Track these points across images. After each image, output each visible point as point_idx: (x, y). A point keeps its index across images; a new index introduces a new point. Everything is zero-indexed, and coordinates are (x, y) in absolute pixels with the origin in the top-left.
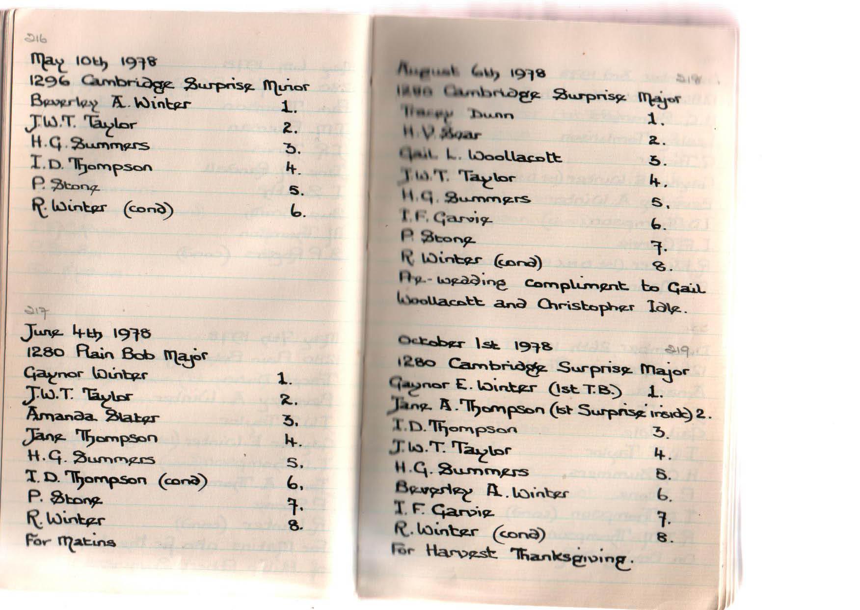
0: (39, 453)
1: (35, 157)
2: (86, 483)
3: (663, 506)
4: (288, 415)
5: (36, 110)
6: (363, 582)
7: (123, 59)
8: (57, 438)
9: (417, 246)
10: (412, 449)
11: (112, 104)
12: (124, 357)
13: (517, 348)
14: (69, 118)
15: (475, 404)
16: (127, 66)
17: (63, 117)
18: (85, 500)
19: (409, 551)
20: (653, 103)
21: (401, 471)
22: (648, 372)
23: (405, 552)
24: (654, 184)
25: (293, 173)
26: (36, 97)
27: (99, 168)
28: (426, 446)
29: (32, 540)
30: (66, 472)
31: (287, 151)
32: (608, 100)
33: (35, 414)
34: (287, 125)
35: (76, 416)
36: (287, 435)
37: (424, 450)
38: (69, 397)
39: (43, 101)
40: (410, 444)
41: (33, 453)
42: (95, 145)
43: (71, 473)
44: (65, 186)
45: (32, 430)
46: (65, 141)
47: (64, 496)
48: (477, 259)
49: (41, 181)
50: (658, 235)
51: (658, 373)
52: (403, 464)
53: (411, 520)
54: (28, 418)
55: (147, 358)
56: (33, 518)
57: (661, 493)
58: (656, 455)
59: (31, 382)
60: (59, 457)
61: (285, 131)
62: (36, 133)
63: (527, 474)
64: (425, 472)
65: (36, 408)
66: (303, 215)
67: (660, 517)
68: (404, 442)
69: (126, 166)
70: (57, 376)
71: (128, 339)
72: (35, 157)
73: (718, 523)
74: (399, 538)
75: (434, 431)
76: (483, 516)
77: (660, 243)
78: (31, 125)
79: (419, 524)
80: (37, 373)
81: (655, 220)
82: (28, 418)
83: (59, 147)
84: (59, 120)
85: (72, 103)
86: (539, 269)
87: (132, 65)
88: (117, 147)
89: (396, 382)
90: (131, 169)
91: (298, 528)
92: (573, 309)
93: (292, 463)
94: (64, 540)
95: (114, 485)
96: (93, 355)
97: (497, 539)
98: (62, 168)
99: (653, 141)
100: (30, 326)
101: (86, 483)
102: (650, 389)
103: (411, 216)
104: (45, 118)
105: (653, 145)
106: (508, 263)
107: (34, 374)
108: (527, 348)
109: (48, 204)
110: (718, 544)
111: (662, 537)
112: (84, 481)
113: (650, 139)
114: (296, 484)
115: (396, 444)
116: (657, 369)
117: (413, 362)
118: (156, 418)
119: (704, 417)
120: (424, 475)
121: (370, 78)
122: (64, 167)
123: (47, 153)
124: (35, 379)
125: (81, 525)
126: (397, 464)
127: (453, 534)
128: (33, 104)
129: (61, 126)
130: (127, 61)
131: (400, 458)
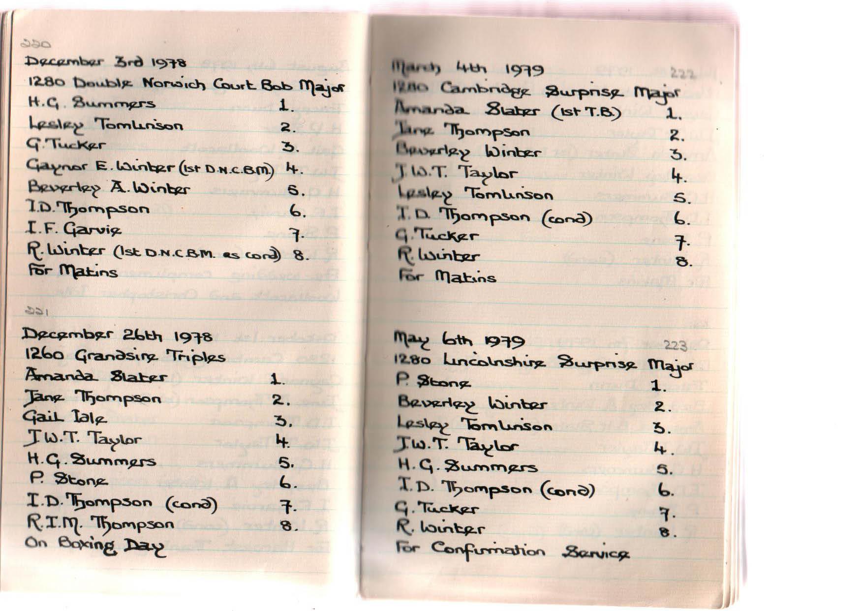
0: (38, 455)
3: (665, 502)
6: (366, 582)
8: (56, 399)
9: (416, 243)
10: (416, 446)
11: (111, 189)
22: (656, 367)
25: (284, 447)
26: (33, 183)
28: (60, 436)
29: (51, 229)
34: (674, 132)
35: (77, 376)
38: (75, 440)
42: (97, 461)
45: (32, 392)
51: (667, 368)
52: (407, 460)
53: (417, 516)
54: (27, 379)
56: (34, 521)
57: (663, 489)
59: (30, 425)
60: (57, 461)
62: (403, 455)
64: (431, 469)
65: (36, 369)
72: (32, 495)
73: (721, 518)
74: (401, 536)
76: (460, 386)
79: (422, 523)
80: (37, 417)
82: (27, 379)
84: (429, 170)
89: (33, 164)
92: (157, 128)
93: (284, 462)
94: (66, 268)
97: (545, 223)
99: (659, 407)
102: (281, 103)
104: (46, 434)
107: (34, 417)
109: (43, 248)
110: (722, 538)
111: (664, 532)
115: (401, 440)
116: (666, 364)
120: (429, 471)
121: (368, 192)
124: (35, 423)
125: (83, 500)
126: (400, 460)
127: (458, 532)
128: (31, 190)
130: (181, 335)
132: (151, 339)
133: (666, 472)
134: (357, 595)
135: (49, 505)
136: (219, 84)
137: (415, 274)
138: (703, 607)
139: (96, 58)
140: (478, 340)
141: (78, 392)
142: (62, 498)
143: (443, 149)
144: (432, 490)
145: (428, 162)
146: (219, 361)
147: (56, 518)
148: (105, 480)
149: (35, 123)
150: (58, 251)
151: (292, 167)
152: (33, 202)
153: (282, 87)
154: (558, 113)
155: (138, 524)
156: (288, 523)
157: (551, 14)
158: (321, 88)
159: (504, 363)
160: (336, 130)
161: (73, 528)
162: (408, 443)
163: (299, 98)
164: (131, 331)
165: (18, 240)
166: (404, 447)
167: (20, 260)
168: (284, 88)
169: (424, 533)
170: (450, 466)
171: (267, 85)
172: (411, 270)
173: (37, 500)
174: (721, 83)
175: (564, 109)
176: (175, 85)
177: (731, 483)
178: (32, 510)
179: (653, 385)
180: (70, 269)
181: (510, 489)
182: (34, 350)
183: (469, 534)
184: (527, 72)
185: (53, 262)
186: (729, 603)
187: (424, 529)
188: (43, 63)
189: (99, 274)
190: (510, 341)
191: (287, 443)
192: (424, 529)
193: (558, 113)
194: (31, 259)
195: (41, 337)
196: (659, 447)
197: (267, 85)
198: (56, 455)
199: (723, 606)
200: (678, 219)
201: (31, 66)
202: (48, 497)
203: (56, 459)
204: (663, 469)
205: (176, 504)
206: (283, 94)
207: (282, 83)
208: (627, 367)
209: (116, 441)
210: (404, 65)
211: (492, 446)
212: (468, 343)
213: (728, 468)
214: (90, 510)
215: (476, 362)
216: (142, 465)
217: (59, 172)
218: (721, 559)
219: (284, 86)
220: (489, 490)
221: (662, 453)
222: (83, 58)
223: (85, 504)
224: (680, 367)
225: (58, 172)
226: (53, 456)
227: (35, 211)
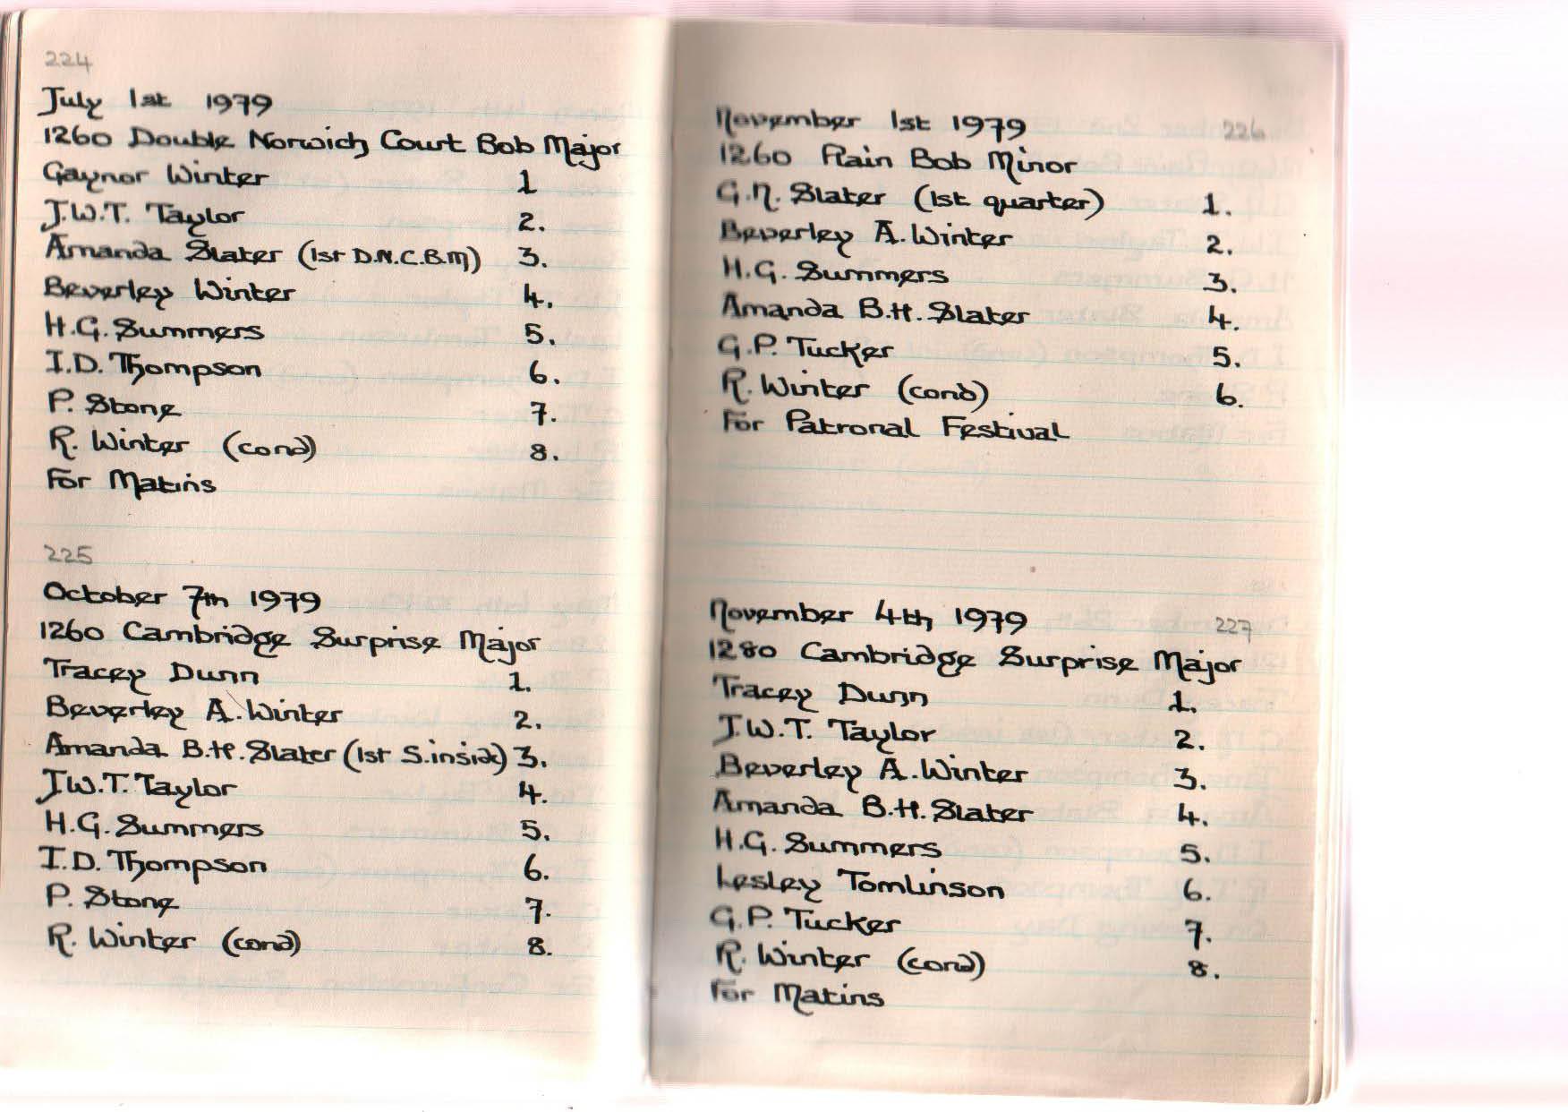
1: (56, 354)
2: (147, 871)
3: (1194, 910)
5: (55, 762)
6: (660, 1053)
7: (956, 119)
10: (75, 788)
14: (116, 207)
16: (215, 109)
17: (106, 206)
18: (145, 900)
19: (755, 424)
20: (1187, 674)
23: (748, 426)
26: (53, 282)
27: (168, 371)
31: (530, 341)
32: (1095, 658)
33: (61, 248)
34: (521, 716)
39: (69, 707)
40: (749, 723)
41: (56, 818)
43: (116, 854)
44: (113, 406)
46: (109, 823)
47: (107, 401)
49: (63, 891)
50: (536, 890)
55: (957, 167)
56: (59, 937)
61: (522, 227)
62: (55, 806)
63: (261, 833)
68: (739, 717)
69: (217, 861)
70: (100, 179)
78: (51, 221)
85: (122, 291)
86: (978, 977)
89: (53, 171)
91: (543, 952)
93: (532, 831)
94: (118, 477)
96: (157, 789)
98: (101, 371)
100: (53, 91)
102: (1207, 201)
105: (1213, 254)
106: (927, 965)
108: (274, 602)
110: (1308, 978)
111: (1198, 969)
112: (145, 867)
114: (539, 873)
115: (726, 722)
117: (737, 651)
118: (276, 254)
119: (1220, 252)
122: (104, 369)
129: (102, 218)
130: (261, 596)
131: (732, 746)
132: (95, 602)
133: (1198, 858)
134: (644, 1080)
135: (77, 867)
136: (392, 140)
138: (1274, 1102)
139: (848, 114)
140: (943, 617)
141: (791, 723)
143: (805, 230)
144: (1208, 899)
150: (110, 443)
151: (1218, 317)
152: (56, 354)
153: (516, 148)
154: (926, 199)
155: (195, 863)
156: (1200, 966)
158: (581, 149)
159: (407, 643)
160: (603, 229)
163: (547, 167)
165: (32, 421)
166: (55, 791)
167: (34, 457)
168: (520, 151)
169: (96, 950)
170: (793, 843)
171: (490, 144)
174: (1312, 151)
175: (937, 195)
176: (310, 146)
177: (1325, 879)
180: (130, 480)
181: (966, 889)
183: (171, 949)
184: (242, 107)
185: (96, 466)
186: (1320, 1093)
187: (97, 941)
189: (182, 488)
190: (1003, 621)
191: (539, 795)
192: (97, 941)
193: (926, 199)
194: (56, 459)
195: (75, 714)
196: (1186, 813)
197: (490, 144)
198: (760, 834)
199: (1309, 1100)
200: (535, 373)
203: (761, 840)
204: (1191, 853)
206: (518, 161)
207: (516, 138)
208: (424, 647)
209: (186, 791)
210: (729, 114)
211: (190, 788)
212: (220, 603)
213: (1319, 849)
216: (912, 853)
217: (96, 185)
218: (1306, 1017)
219: (520, 147)
220: (191, 866)
221: (1192, 824)
222: (819, 114)
224: (1213, 664)
225: (95, 186)
226: (767, 265)
227: (61, 370)
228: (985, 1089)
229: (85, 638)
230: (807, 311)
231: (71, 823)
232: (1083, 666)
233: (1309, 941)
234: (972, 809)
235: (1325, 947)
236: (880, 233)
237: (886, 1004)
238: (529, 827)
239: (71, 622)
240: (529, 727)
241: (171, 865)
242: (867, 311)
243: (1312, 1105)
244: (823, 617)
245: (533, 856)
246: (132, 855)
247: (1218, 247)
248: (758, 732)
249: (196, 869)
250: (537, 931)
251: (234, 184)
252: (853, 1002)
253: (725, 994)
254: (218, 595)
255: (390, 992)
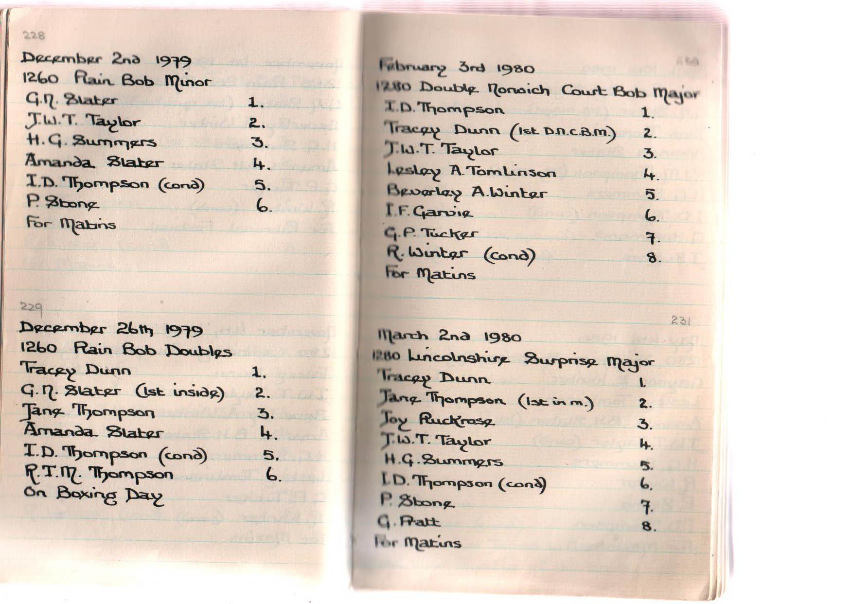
3: (646, 494)
4: (262, 408)
6: (356, 571)
7: (499, 66)
12: (125, 353)
13: (487, 339)
14: (35, 115)
15: (77, 180)
21: (390, 462)
24: (644, 447)
30: (414, 477)
33: (33, 160)
34: (253, 120)
36: (262, 427)
37: (411, 442)
48: (461, 252)
49: (35, 198)
50: (652, 227)
54: (25, 433)
58: (642, 445)
59: (33, 108)
61: (251, 125)
65: (34, 423)
66: (269, 209)
67: (644, 506)
71: (497, 343)
72: (31, 176)
75: (419, 424)
77: (653, 234)
81: (261, 200)
82: (25, 433)
83: (37, 102)
87: (165, 63)
88: (46, 433)
90: (535, 175)
95: (462, 487)
101: (109, 478)
103: (394, 210)
111: (646, 526)
113: (251, 121)
119: (650, 137)
123: (43, 109)
126: (386, 456)
130: (491, 335)
131: (389, 451)
137: (400, 270)
142: (57, 180)
145: (415, 139)
146: (407, 173)
147: (55, 467)
148: (96, 203)
149: (393, 168)
157: (541, 12)
161: (70, 478)
162: (397, 148)
164: (126, 325)
172: (397, 266)
173: (34, 450)
174: (713, 82)
178: (31, 190)
179: (254, 372)
182: (30, 344)
186: (716, 595)
188: (38, 60)
195: (37, 331)
198: (411, 456)
201: (28, 62)
202: (45, 179)
205: (169, 456)
214: (86, 462)
215: (440, 358)
223: (82, 454)
228: (533, 591)
229: (46, 348)
230: (192, 186)
231: (398, 458)
232: (650, 364)
233: (710, 513)
234: (131, 432)
235: (718, 517)
236: (28, 160)
237: (462, 546)
238: (268, 454)
239: (39, 343)
240: (264, 397)
241: (123, 475)
242: (126, 82)
243: (711, 601)
244: (92, 330)
245: (270, 468)
246: (85, 407)
247: (649, 134)
248: (403, 441)
249: (112, 457)
250: (646, 518)
251: (100, 104)
252: (446, 545)
253: (394, 274)
254: (148, 327)
255: (177, 543)
